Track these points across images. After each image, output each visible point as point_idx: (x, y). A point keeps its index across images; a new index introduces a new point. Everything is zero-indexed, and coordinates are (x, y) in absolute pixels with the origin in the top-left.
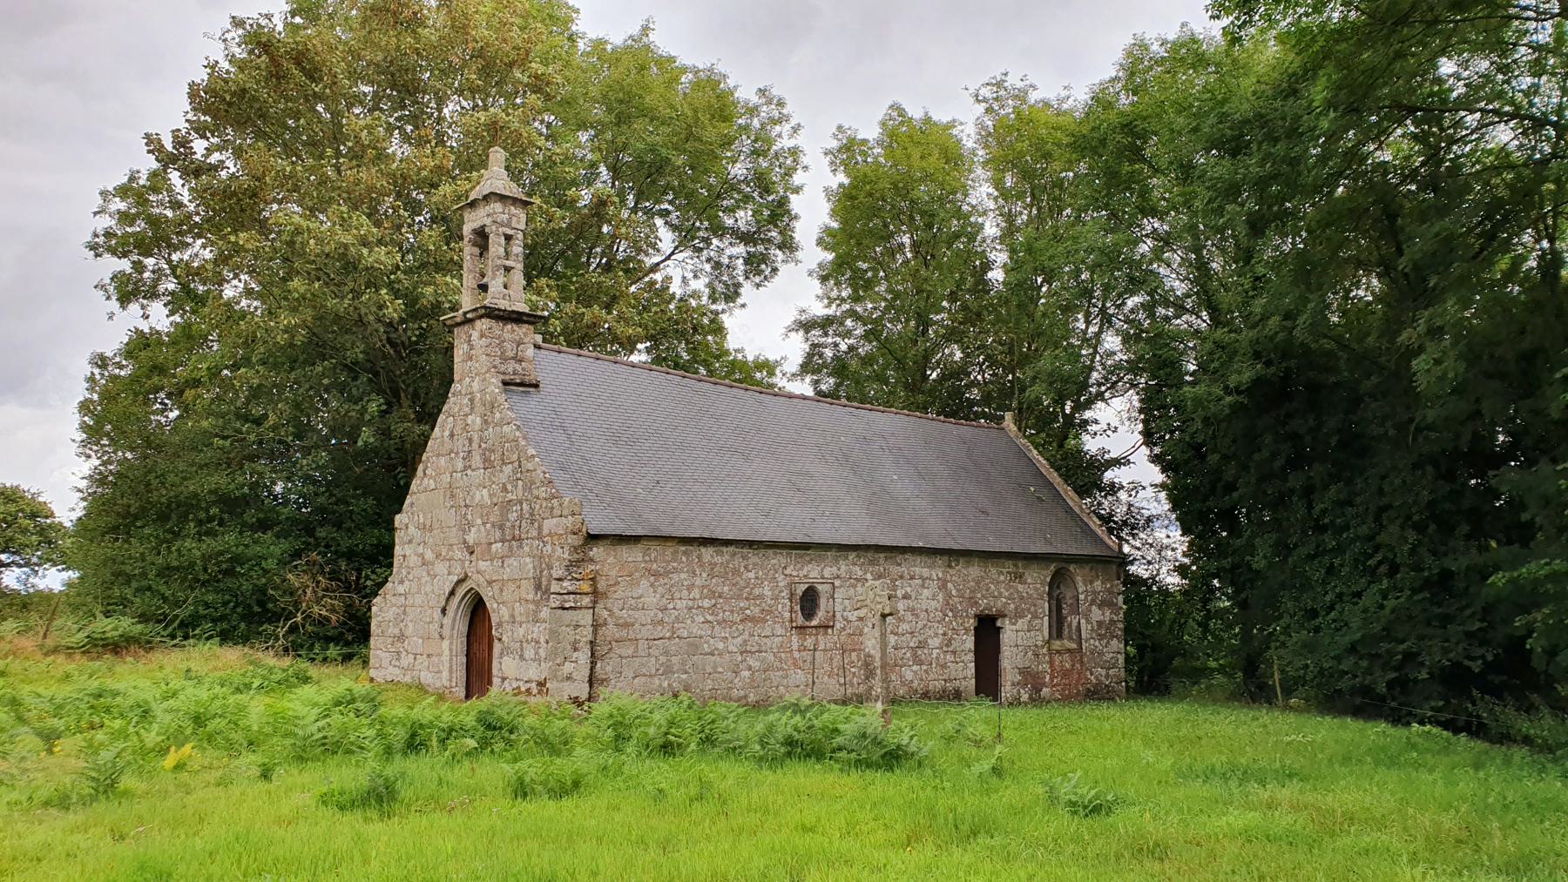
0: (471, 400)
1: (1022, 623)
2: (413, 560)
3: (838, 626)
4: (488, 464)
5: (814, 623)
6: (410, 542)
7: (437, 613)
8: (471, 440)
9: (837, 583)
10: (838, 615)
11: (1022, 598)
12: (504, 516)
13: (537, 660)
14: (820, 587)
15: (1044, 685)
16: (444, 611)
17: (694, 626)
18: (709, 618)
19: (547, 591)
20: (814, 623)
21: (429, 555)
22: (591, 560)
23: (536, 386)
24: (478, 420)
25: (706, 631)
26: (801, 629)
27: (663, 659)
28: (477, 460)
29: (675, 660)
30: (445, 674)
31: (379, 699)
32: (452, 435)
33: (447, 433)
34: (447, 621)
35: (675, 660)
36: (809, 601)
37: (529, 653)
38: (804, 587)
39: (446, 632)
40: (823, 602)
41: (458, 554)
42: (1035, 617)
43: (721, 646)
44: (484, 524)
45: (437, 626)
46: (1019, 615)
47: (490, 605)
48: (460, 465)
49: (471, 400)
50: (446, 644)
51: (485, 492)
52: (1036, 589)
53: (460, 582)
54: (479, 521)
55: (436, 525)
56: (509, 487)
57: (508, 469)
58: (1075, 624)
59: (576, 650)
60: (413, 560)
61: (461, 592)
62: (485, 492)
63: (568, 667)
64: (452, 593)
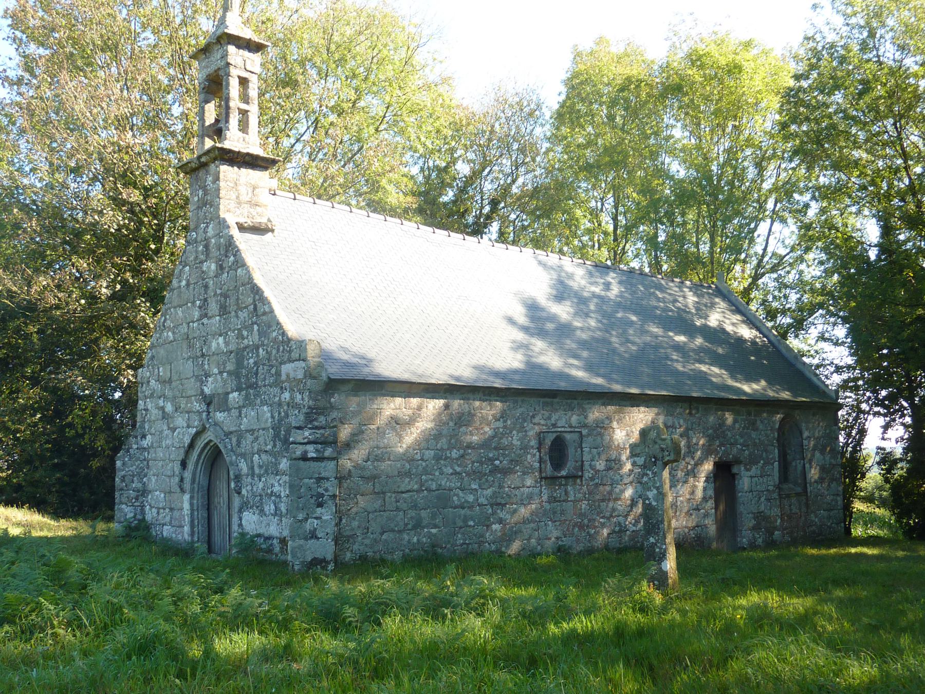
0: (206, 246)
1: (754, 470)
2: (154, 413)
3: (587, 475)
4: (224, 310)
5: (563, 473)
6: (152, 396)
7: (177, 468)
8: (206, 287)
9: (585, 432)
10: (586, 464)
11: (755, 444)
12: (239, 363)
13: (277, 513)
14: (568, 437)
15: (776, 528)
16: (184, 464)
17: (162, 139)
18: (458, 469)
19: (286, 442)
20: (563, 473)
21: (169, 408)
22: (332, 407)
23: (272, 231)
24: (213, 266)
25: (454, 483)
26: (552, 480)
27: (412, 513)
28: (213, 307)
29: (424, 514)
30: (187, 529)
31: (782, 237)
32: (188, 285)
33: (184, 283)
34: (188, 475)
35: (424, 514)
36: (557, 451)
37: (270, 508)
38: (552, 437)
39: (187, 486)
40: (571, 451)
41: (197, 406)
42: (767, 463)
43: (471, 498)
44: (221, 373)
45: (177, 479)
46: (753, 461)
47: (229, 458)
48: (196, 314)
49: (206, 246)
50: (187, 497)
51: (221, 340)
52: (767, 436)
53: (198, 434)
54: (216, 371)
55: (175, 377)
56: (245, 333)
57: (243, 315)
58: (800, 468)
59: (320, 505)
60: (154, 413)
61: (200, 444)
62: (221, 340)
63: (311, 524)
64: (191, 445)
